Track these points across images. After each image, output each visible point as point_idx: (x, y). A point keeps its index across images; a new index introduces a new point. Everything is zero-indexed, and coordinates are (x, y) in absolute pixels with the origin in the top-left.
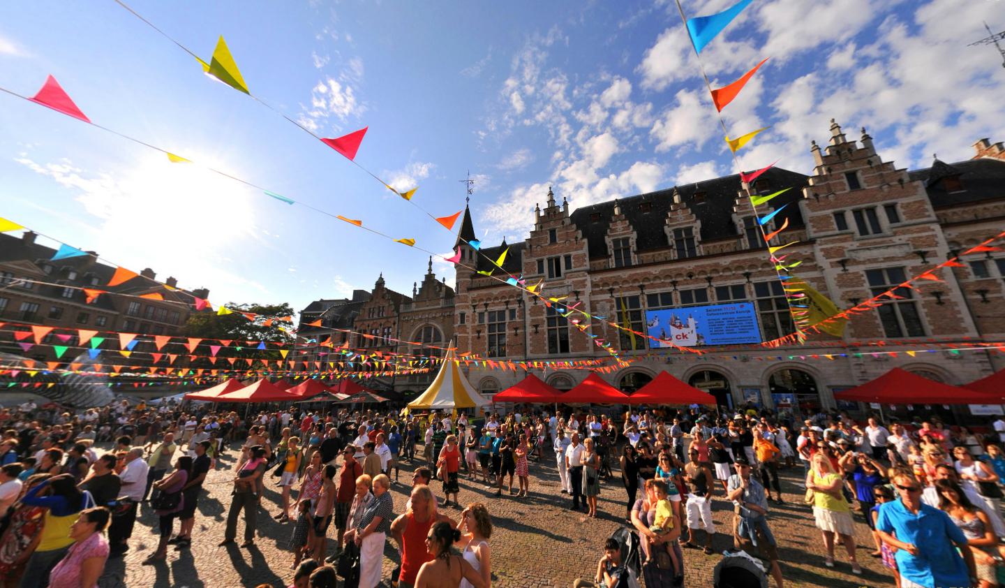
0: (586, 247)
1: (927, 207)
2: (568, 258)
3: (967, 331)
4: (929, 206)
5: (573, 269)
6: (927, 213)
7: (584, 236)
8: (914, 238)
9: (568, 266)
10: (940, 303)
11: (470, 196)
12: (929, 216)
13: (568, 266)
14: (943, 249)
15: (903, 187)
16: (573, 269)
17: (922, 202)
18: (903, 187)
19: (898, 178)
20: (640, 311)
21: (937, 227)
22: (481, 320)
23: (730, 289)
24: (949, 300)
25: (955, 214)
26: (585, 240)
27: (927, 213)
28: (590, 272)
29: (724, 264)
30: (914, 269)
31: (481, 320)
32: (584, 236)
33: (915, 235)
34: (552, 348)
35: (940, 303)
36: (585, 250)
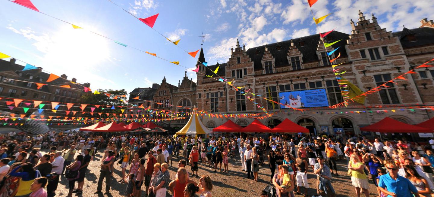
0: (253, 65)
1: (400, 48)
2: (245, 70)
3: (418, 101)
4: (401, 48)
5: (247, 75)
6: (400, 51)
7: (252, 61)
8: (395, 61)
9: (245, 73)
10: (406, 89)
11: (203, 43)
12: (401, 52)
13: (245, 73)
14: (407, 66)
15: (390, 39)
16: (247, 75)
17: (398, 46)
18: (390, 39)
19: (388, 35)
20: (276, 93)
21: (405, 57)
22: (208, 96)
24: (410, 88)
26: (253, 62)
27: (400, 51)
28: (255, 76)
29: (312, 72)
30: (395, 75)
31: (208, 96)
32: (252, 61)
33: (395, 60)
34: (239, 108)
35: (406, 89)
36: (253, 66)
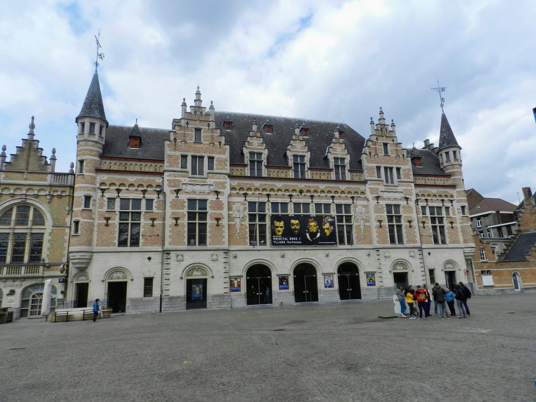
14: (414, 198)
17: (409, 169)
21: (413, 185)
23: (323, 206)
25: (106, 165)
26: (228, 147)
29: (256, 185)
36: (226, 156)
